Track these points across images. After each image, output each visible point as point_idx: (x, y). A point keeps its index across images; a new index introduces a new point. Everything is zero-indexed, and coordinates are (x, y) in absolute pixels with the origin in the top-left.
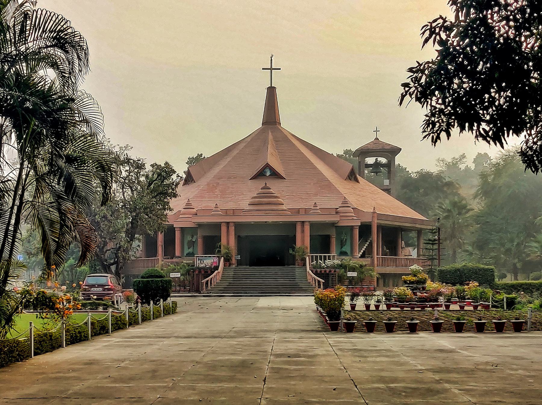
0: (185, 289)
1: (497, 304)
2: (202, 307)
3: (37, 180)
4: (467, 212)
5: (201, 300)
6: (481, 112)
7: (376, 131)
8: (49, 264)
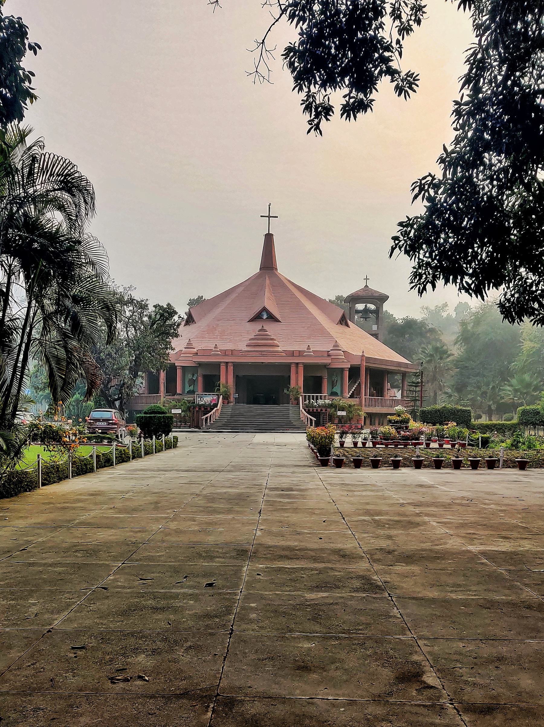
0: (185, 425)
1: (473, 444)
2: (201, 442)
3: (44, 319)
4: (448, 357)
5: (201, 436)
6: (465, 265)
7: (367, 279)
8: (55, 400)
